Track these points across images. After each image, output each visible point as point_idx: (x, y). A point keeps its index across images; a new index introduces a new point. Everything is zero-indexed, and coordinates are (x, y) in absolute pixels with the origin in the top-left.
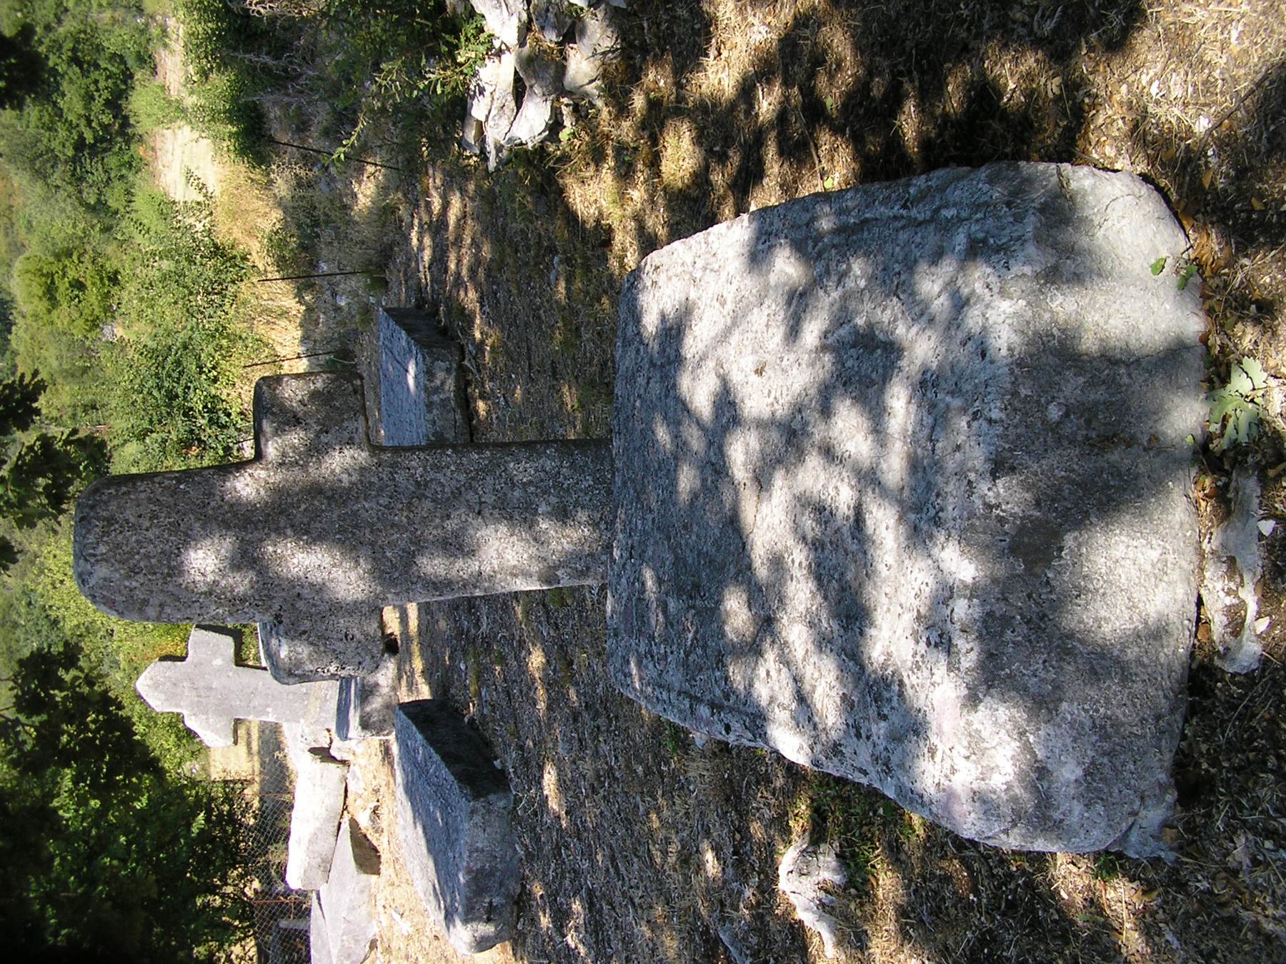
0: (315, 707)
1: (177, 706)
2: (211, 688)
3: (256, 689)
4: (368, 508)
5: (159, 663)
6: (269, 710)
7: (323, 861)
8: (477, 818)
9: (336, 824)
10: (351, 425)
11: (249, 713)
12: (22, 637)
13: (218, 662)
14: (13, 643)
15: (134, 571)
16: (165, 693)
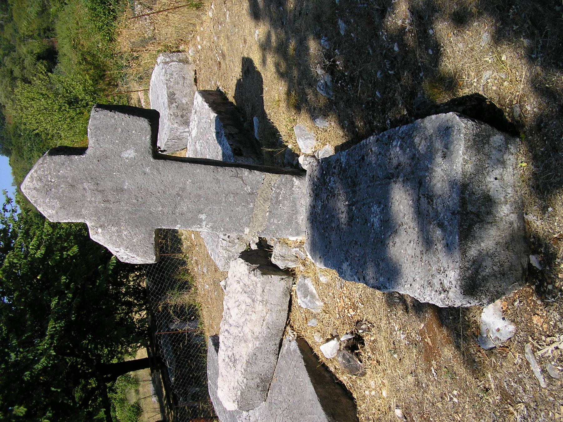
0: (264, 211)
1: (78, 216)
2: (122, 190)
3: (183, 189)
5: (48, 158)
6: (203, 217)
7: (262, 381)
9: (278, 342)
11: (176, 223)
12: (23, 141)
13: (129, 154)
14: (19, 144)
16: (60, 199)
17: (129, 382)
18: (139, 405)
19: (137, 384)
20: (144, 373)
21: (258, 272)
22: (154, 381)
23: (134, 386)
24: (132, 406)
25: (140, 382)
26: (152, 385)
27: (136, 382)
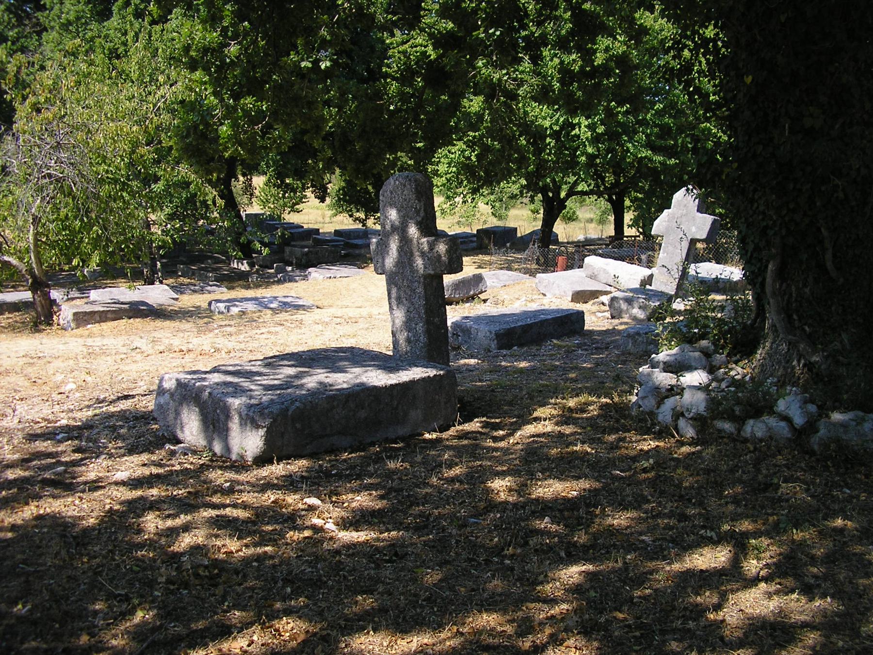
1: (674, 206)
4: (408, 272)
6: (665, 255)
8: (488, 333)
10: (430, 268)
15: (391, 193)
17: (604, 213)
18: (574, 220)
19: (600, 222)
20: (610, 231)
21: (643, 278)
22: (600, 239)
23: (598, 218)
24: (574, 212)
25: (601, 226)
26: (596, 236)
27: (602, 221)
